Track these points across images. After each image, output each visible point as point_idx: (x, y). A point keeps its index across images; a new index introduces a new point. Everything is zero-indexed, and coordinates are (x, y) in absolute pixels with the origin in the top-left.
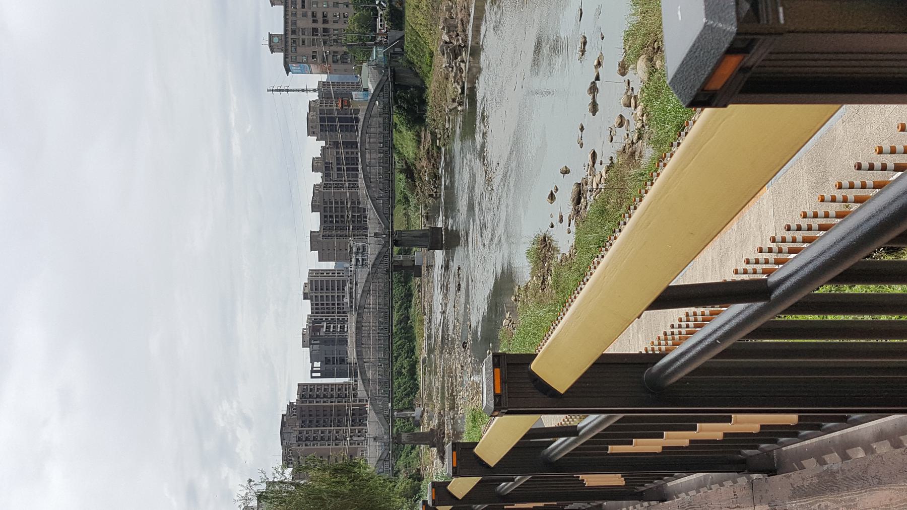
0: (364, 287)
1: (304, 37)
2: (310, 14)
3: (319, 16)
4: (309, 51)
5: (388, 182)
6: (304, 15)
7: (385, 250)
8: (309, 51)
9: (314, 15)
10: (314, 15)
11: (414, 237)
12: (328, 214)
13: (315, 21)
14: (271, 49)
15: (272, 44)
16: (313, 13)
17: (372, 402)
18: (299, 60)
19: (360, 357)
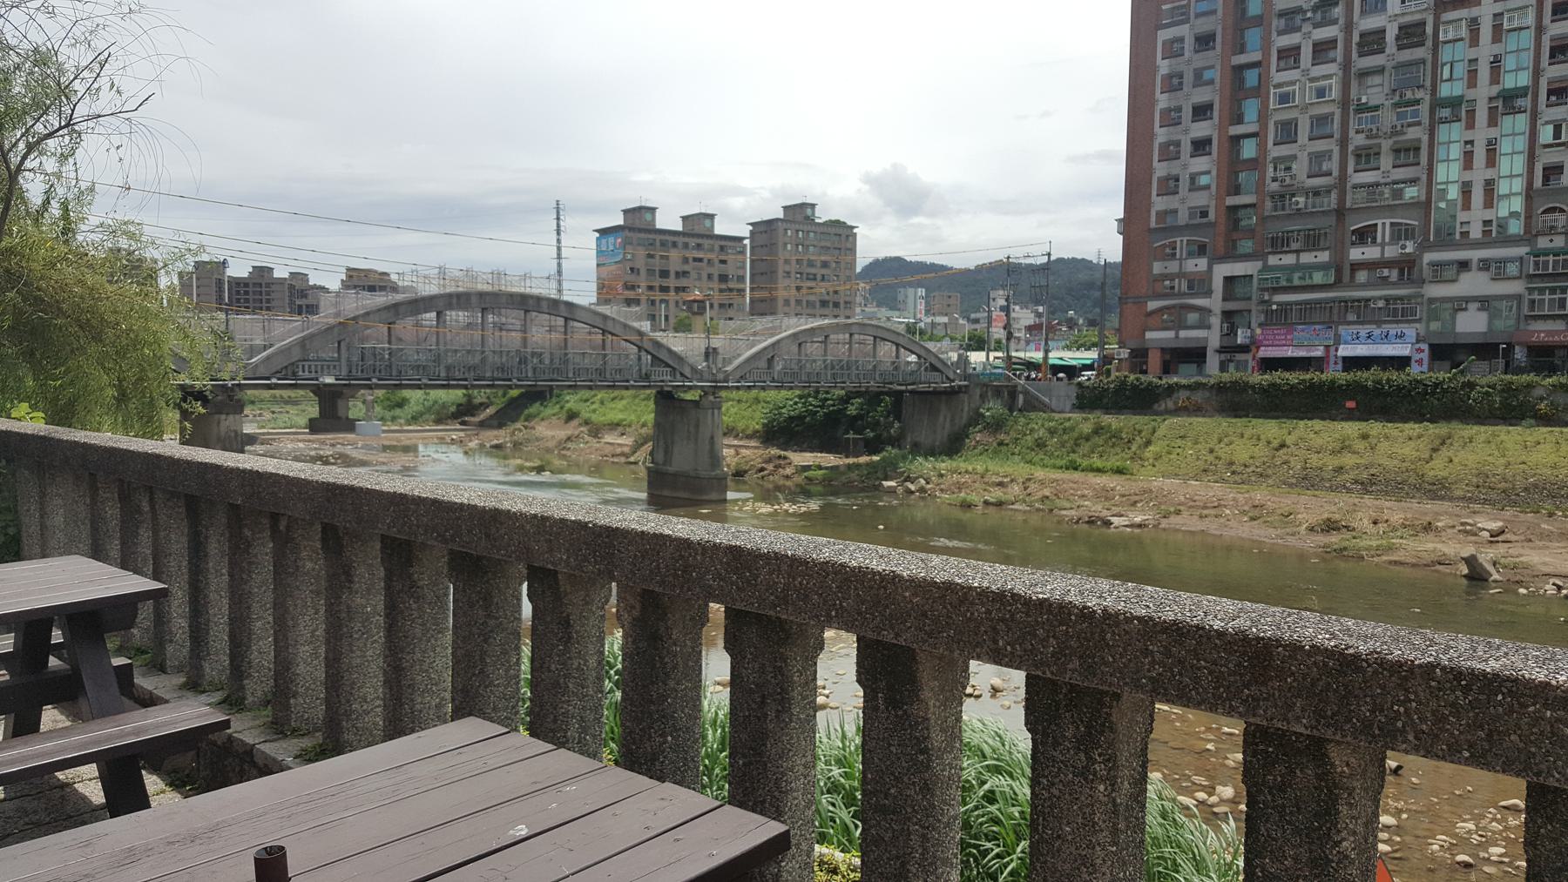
0: (614, 319)
1: (658, 257)
2: (686, 268)
3: (683, 282)
4: (640, 263)
5: (443, 374)
6: (686, 261)
7: (687, 372)
8: (640, 263)
9: (685, 274)
10: (685, 274)
11: (712, 438)
12: (250, 289)
13: (677, 274)
14: (634, 210)
15: (643, 211)
16: (688, 272)
17: (336, 330)
18: (630, 249)
19: (455, 301)
